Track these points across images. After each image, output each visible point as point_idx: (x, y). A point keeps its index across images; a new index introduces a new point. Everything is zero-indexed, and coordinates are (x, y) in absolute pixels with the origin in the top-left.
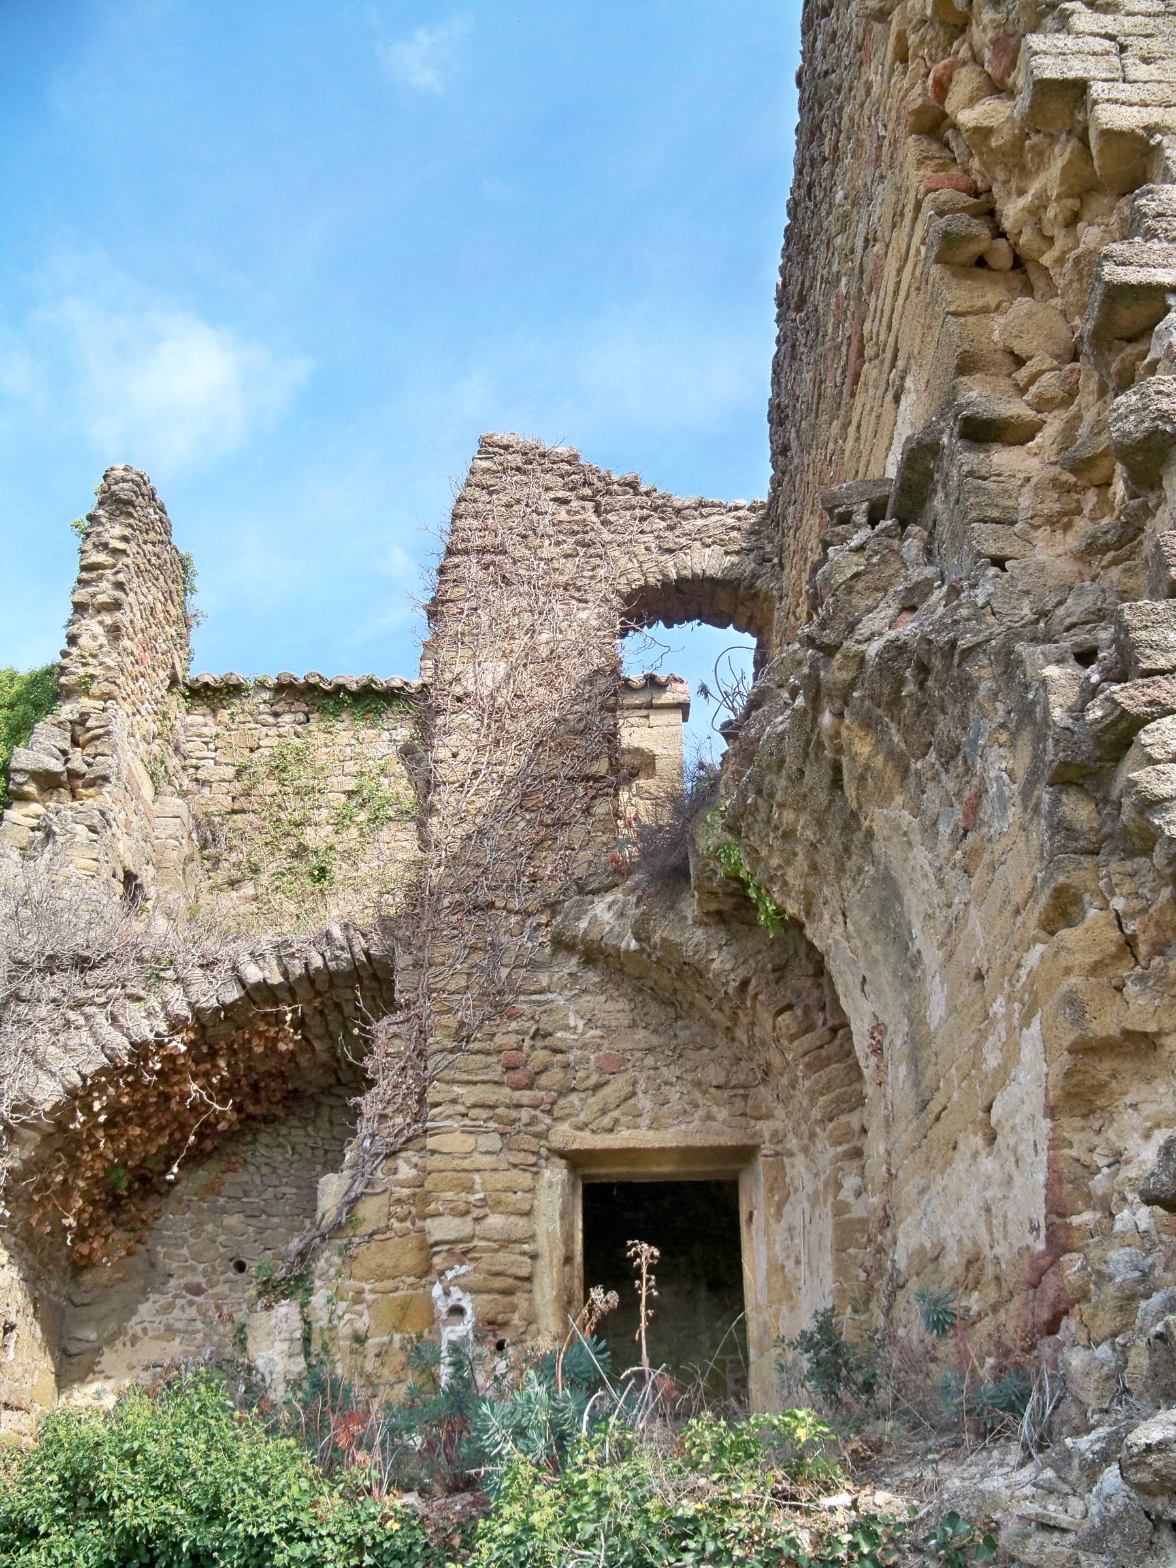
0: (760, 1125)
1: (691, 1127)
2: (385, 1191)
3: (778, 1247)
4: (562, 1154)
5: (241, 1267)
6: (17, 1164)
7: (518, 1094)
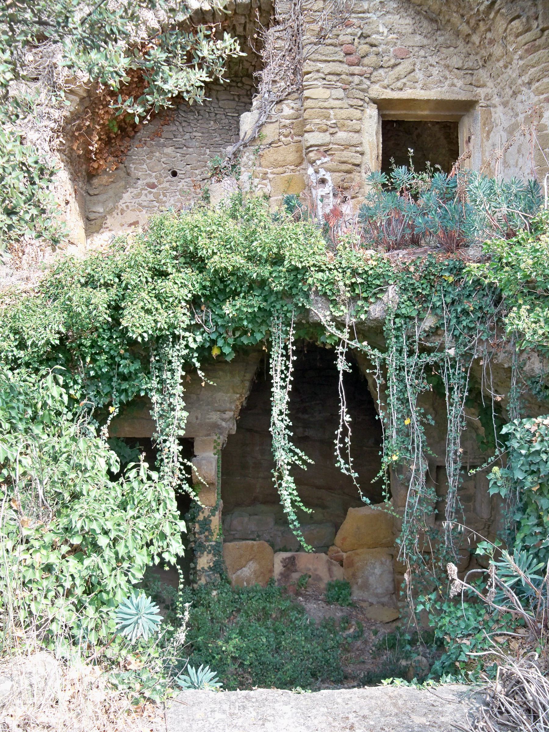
0: (479, 90)
1: (444, 89)
2: (277, 121)
3: (487, 154)
4: (374, 101)
5: (174, 174)
6: (68, 114)
7: (352, 68)
